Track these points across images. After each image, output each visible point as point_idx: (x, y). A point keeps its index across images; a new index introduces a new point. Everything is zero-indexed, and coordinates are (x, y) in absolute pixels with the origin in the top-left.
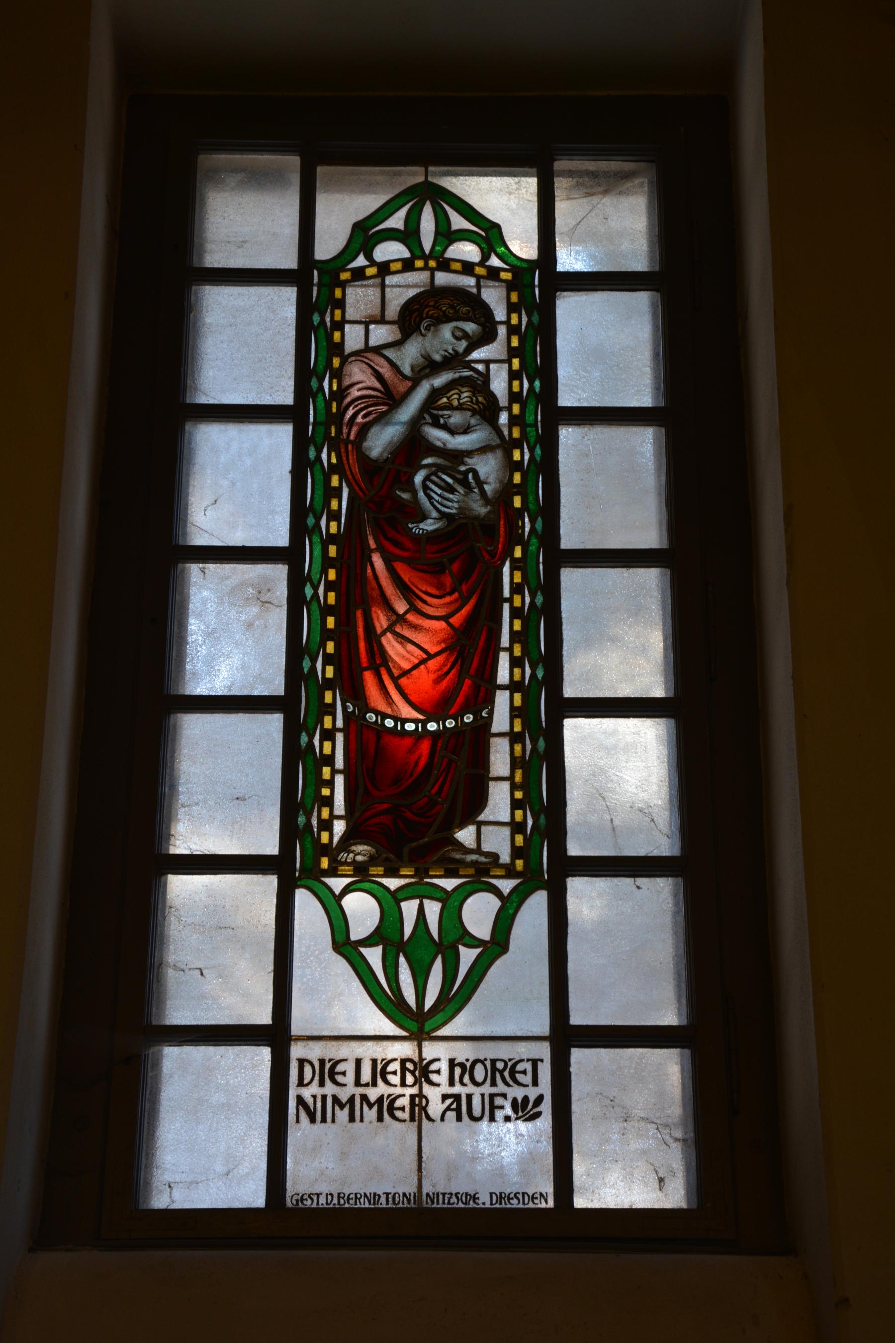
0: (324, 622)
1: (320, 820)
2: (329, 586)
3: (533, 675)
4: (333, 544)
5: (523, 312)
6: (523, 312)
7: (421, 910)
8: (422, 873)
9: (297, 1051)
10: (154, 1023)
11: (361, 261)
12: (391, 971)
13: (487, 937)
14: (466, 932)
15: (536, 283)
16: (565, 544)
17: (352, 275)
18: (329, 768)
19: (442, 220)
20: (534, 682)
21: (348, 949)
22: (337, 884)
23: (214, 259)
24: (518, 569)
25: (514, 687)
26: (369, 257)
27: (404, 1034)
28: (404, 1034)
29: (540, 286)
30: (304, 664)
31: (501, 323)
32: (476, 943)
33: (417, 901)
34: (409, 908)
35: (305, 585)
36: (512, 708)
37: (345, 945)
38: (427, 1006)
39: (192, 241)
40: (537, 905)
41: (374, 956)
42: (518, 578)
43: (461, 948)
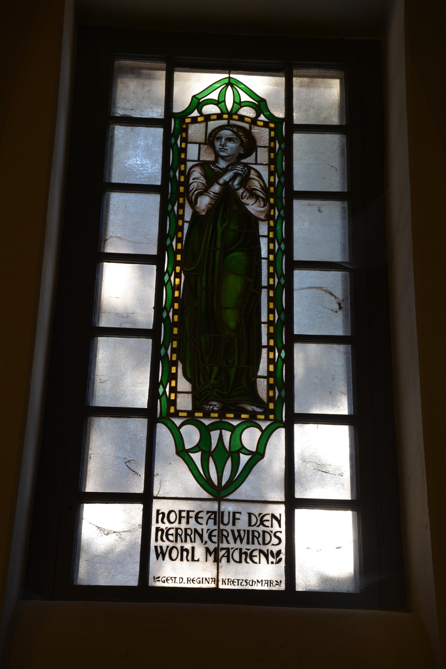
0: (173, 294)
1: (171, 388)
2: (174, 351)
3: (279, 282)
4: (176, 327)
5: (276, 389)
6: (276, 389)
7: (221, 437)
8: (222, 414)
9: (157, 505)
10: (90, 405)
11: (195, 113)
12: (205, 467)
13: (254, 450)
14: (243, 447)
15: (284, 196)
16: (296, 332)
17: (192, 120)
18: (181, 221)
19: (236, 95)
20: (279, 285)
21: (183, 453)
22: (178, 422)
23: (116, 178)
24: (271, 338)
25: (270, 287)
26: (200, 112)
27: (211, 497)
28: (211, 497)
29: (286, 198)
30: (161, 352)
31: (264, 258)
32: (247, 452)
33: (219, 431)
34: (215, 435)
35: (167, 239)
36: (269, 297)
37: (182, 452)
38: (223, 483)
39: (90, 378)
40: (280, 435)
41: (197, 457)
42: (271, 270)
43: (241, 455)
